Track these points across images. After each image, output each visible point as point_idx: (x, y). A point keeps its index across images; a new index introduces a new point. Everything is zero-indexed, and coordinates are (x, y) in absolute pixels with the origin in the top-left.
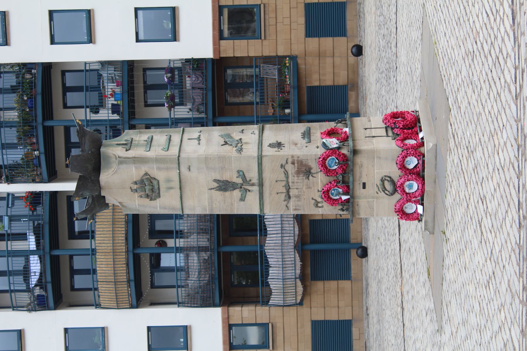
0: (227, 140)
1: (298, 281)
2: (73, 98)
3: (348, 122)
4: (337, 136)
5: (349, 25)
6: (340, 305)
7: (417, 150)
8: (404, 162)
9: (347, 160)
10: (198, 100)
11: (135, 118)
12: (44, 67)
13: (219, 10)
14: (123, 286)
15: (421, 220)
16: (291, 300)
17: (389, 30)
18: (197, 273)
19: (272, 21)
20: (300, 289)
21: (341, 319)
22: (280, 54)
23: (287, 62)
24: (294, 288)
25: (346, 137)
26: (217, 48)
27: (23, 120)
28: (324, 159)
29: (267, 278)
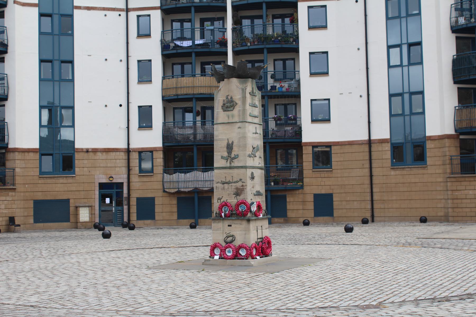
1: (176, 190)
3: (265, 217)
5: (321, 218)
7: (250, 255)
9: (244, 216)
10: (279, 134)
13: (329, 145)
16: (166, 185)
19: (323, 175)
20: (173, 191)
22: (305, 180)
28: (244, 203)
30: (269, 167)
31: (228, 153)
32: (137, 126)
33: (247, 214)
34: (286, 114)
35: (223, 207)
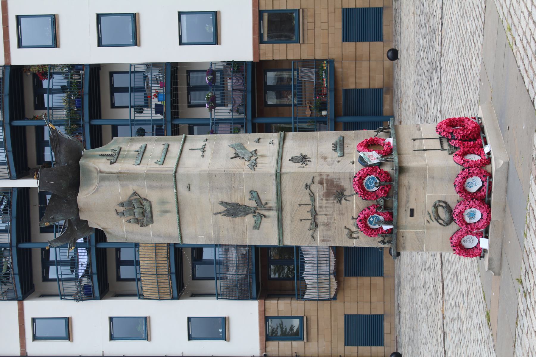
0: (238, 151)
1: (333, 279)
2: (121, 98)
3: (392, 131)
4: (378, 148)
5: (385, 30)
6: (372, 301)
8: (464, 183)
9: (391, 180)
10: (239, 101)
11: (178, 118)
12: (92, 68)
13: (259, 14)
14: (164, 278)
15: (484, 257)
17: (432, 28)
18: (235, 268)
19: (310, 26)
20: (334, 284)
21: (373, 313)
22: (318, 57)
23: (324, 65)
24: (328, 283)
25: (389, 150)
26: (256, 51)
27: (71, 119)
28: (361, 179)
29: (302, 273)
30: (295, 118)
31: (247, 214)
32: (223, 342)
33: (386, 172)
34: (203, 88)
35: (369, 228)
